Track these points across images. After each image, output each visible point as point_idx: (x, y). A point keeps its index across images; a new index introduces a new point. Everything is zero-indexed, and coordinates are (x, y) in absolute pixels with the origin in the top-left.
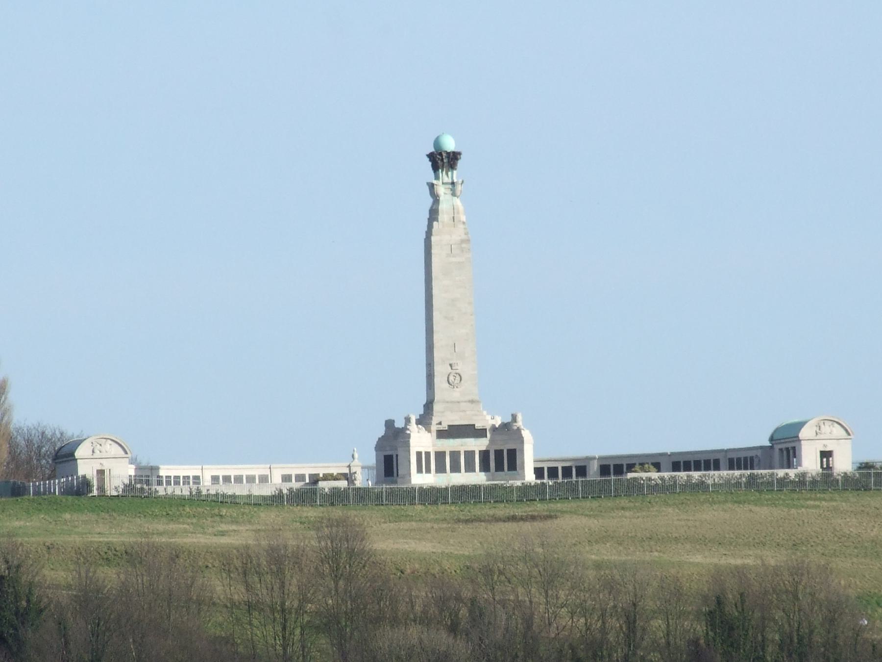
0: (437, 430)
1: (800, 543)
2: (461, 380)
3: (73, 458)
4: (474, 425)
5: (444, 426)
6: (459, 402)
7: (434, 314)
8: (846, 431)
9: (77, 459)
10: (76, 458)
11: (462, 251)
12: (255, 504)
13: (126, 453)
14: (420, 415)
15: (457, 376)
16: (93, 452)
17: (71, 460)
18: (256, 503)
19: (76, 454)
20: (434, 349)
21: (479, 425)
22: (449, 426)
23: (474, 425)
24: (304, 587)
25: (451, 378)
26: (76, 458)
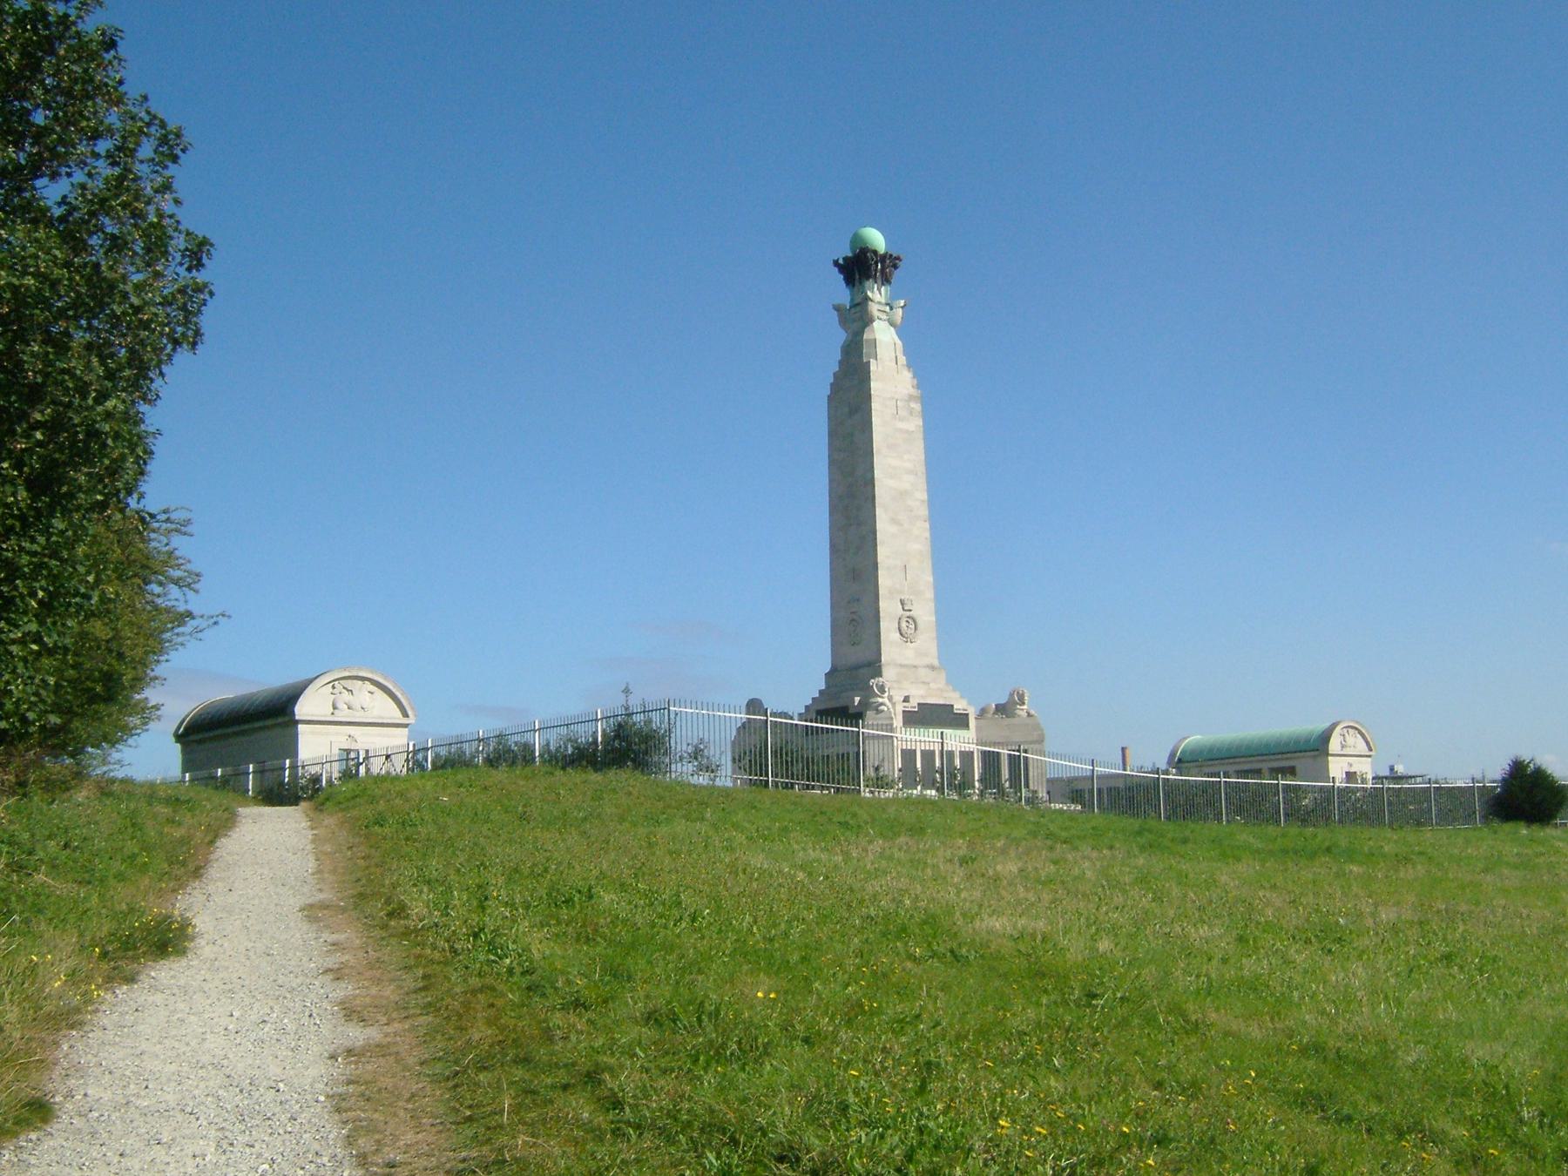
0: (904, 711)
1: (560, 1099)
2: (916, 629)
3: (286, 719)
4: (952, 706)
5: (913, 705)
6: (915, 667)
7: (877, 513)
8: (1367, 743)
9: (297, 722)
10: (297, 718)
11: (911, 413)
12: (942, 738)
13: (406, 715)
14: (806, 707)
15: (910, 621)
16: (335, 708)
17: (261, 728)
18: (876, 742)
19: (297, 709)
20: (880, 572)
21: (959, 707)
22: (919, 704)
23: (952, 706)
24: (365, 1123)
25: (904, 624)
26: (297, 718)
